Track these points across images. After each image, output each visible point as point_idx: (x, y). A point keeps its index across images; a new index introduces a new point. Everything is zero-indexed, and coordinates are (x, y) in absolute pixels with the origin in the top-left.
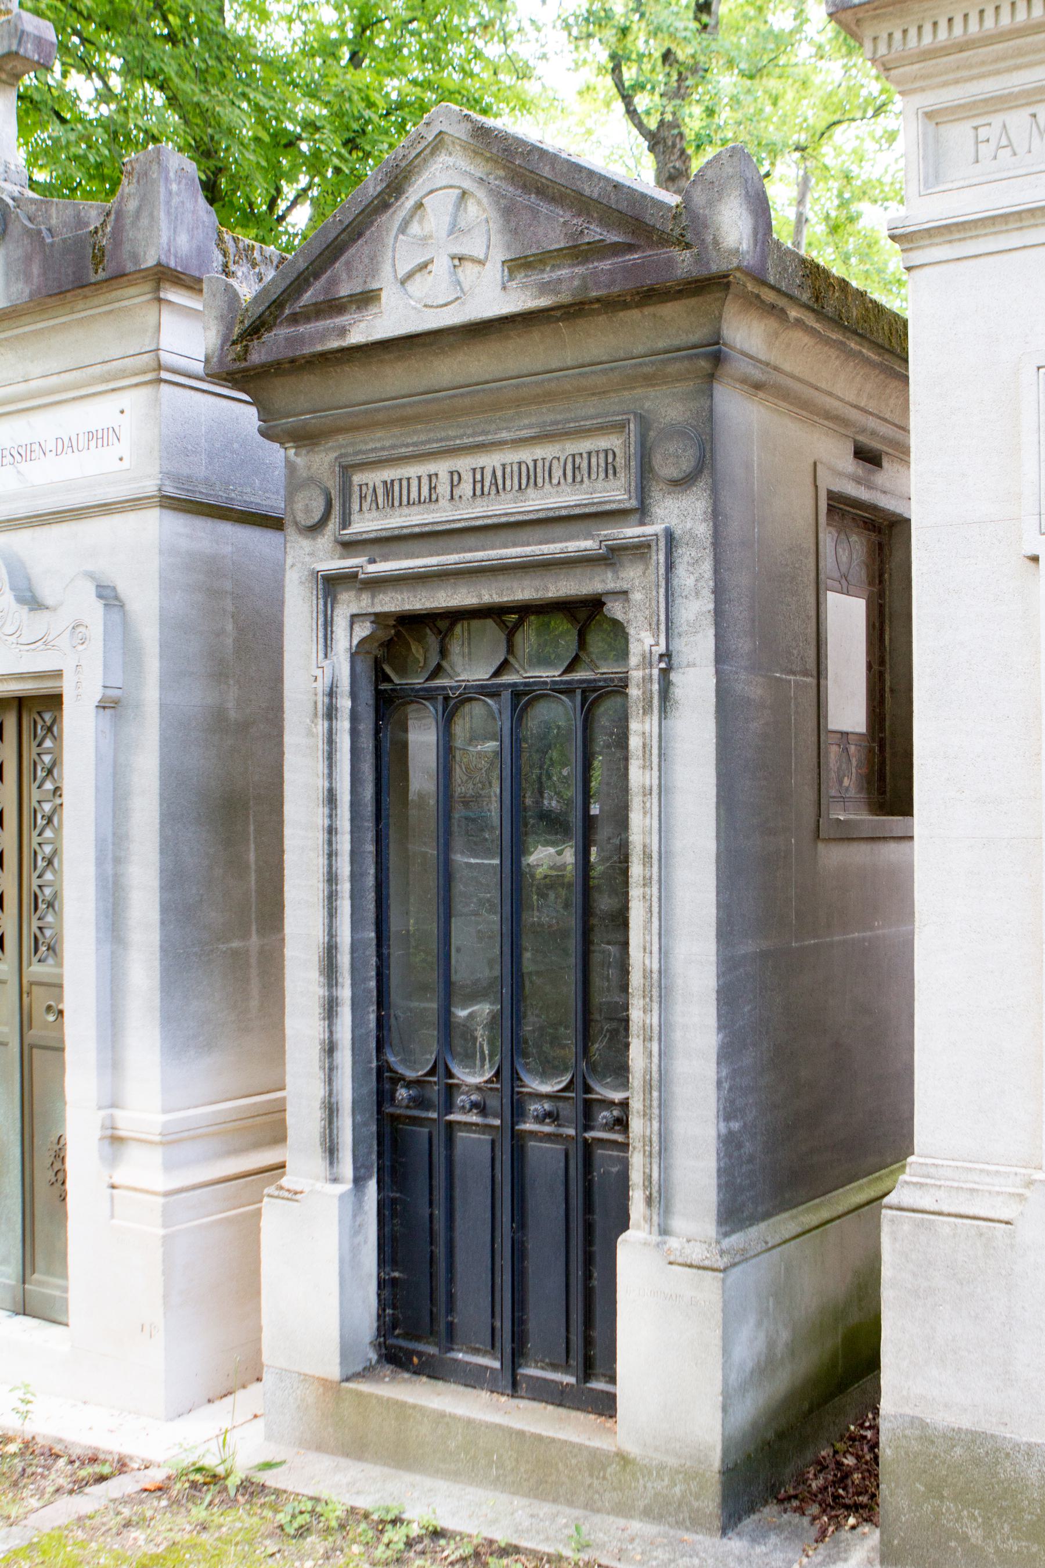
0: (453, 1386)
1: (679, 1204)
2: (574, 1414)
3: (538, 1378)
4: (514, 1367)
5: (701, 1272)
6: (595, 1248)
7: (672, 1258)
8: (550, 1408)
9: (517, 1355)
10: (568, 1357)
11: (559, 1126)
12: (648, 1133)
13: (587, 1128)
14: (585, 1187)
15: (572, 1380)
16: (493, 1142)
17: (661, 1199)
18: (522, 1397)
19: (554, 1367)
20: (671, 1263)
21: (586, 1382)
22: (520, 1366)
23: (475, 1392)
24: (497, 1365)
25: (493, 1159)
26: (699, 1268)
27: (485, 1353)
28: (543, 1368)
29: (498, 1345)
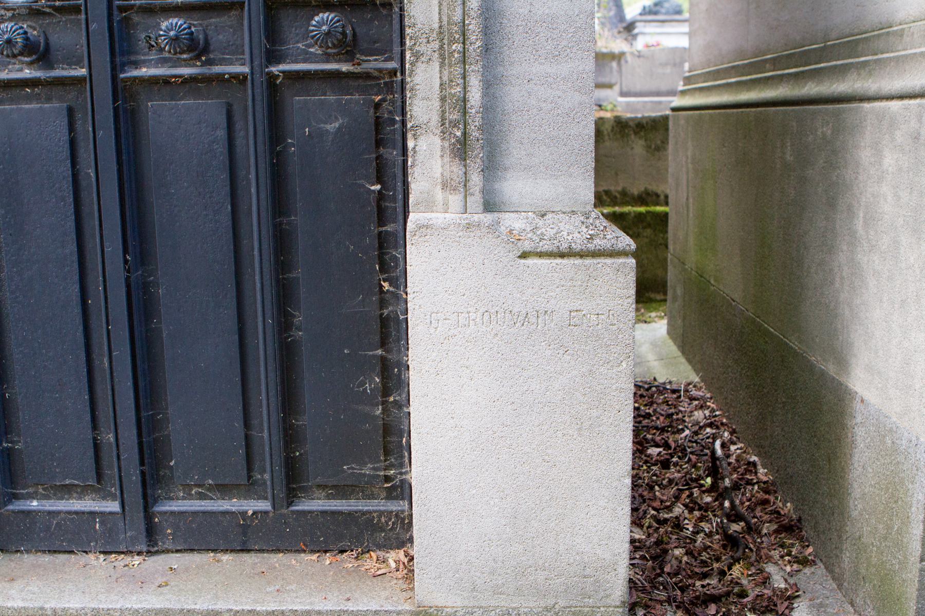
0: (28, 559)
1: (517, 149)
2: (277, 559)
3: (195, 513)
4: (148, 502)
5: (588, 261)
6: (298, 273)
7: (527, 246)
8: (226, 558)
9: (153, 479)
10: (250, 469)
11: (209, 62)
12: (457, 17)
13: (273, 57)
14: (273, 165)
15: (264, 505)
16: (71, 111)
17: (479, 145)
18: (167, 551)
19: (224, 490)
20: (524, 255)
21: (290, 504)
22: (156, 501)
23: (82, 559)
24: (113, 506)
25: (73, 144)
26: (581, 255)
27: (83, 491)
28: (202, 496)
29: (111, 472)
